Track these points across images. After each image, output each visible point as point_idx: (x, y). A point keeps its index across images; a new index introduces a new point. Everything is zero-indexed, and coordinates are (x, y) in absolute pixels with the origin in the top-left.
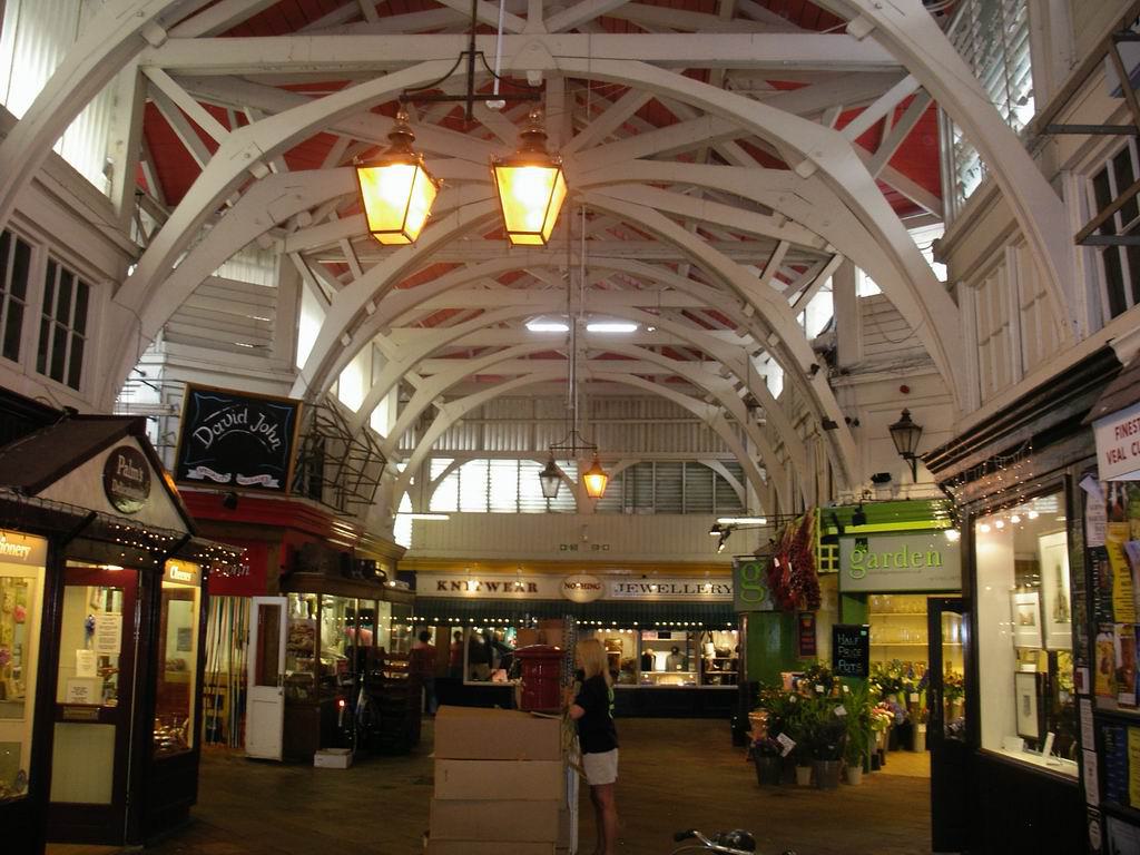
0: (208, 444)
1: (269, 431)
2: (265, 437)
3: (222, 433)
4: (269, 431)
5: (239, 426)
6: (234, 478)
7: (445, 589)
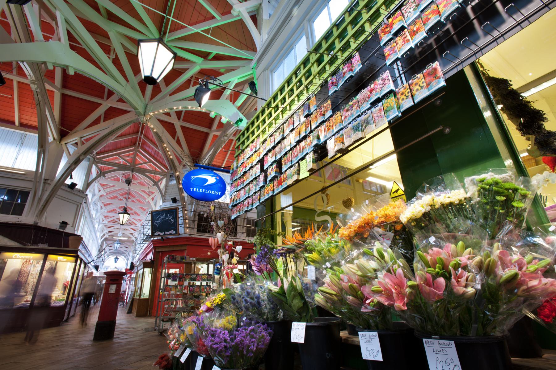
0: (158, 225)
1: (171, 218)
2: (170, 220)
4: (171, 218)
5: (164, 219)
6: (165, 233)
7: (196, 77)
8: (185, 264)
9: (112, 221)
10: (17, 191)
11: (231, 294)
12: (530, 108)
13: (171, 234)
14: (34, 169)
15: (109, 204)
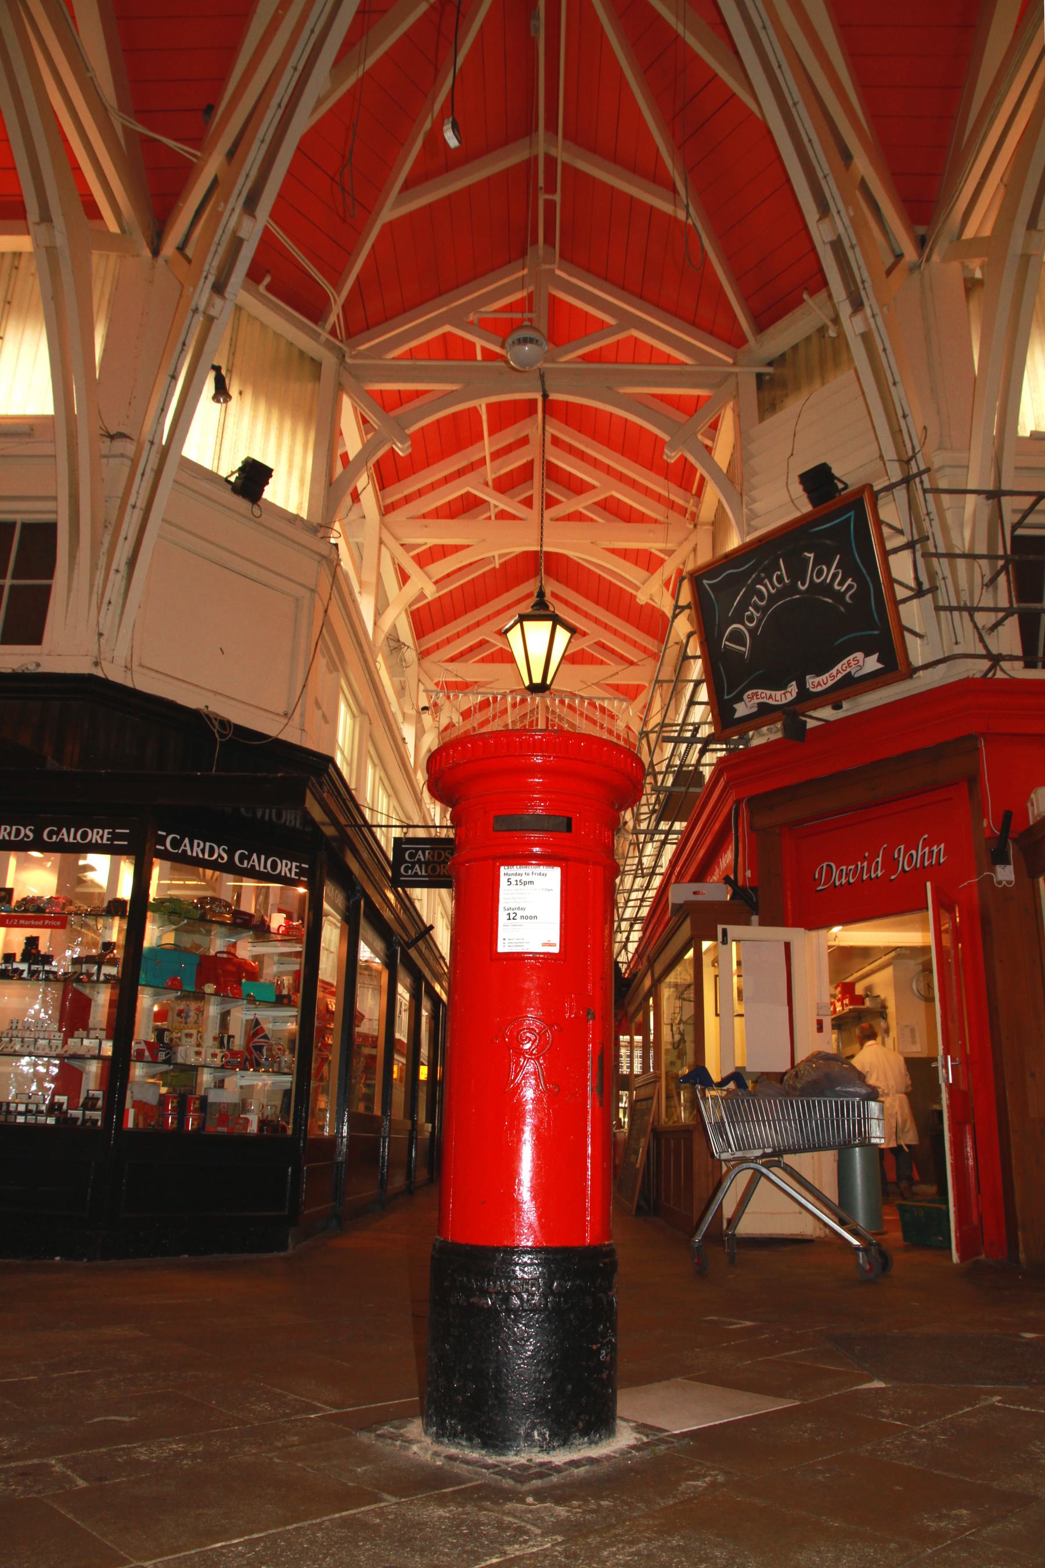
0: (745, 650)
1: (830, 573)
2: (826, 589)
3: (760, 621)
4: (830, 573)
5: (780, 594)
6: (802, 685)
9: (471, 649)
10: (12, 525)
13: (850, 685)
15: (514, 517)
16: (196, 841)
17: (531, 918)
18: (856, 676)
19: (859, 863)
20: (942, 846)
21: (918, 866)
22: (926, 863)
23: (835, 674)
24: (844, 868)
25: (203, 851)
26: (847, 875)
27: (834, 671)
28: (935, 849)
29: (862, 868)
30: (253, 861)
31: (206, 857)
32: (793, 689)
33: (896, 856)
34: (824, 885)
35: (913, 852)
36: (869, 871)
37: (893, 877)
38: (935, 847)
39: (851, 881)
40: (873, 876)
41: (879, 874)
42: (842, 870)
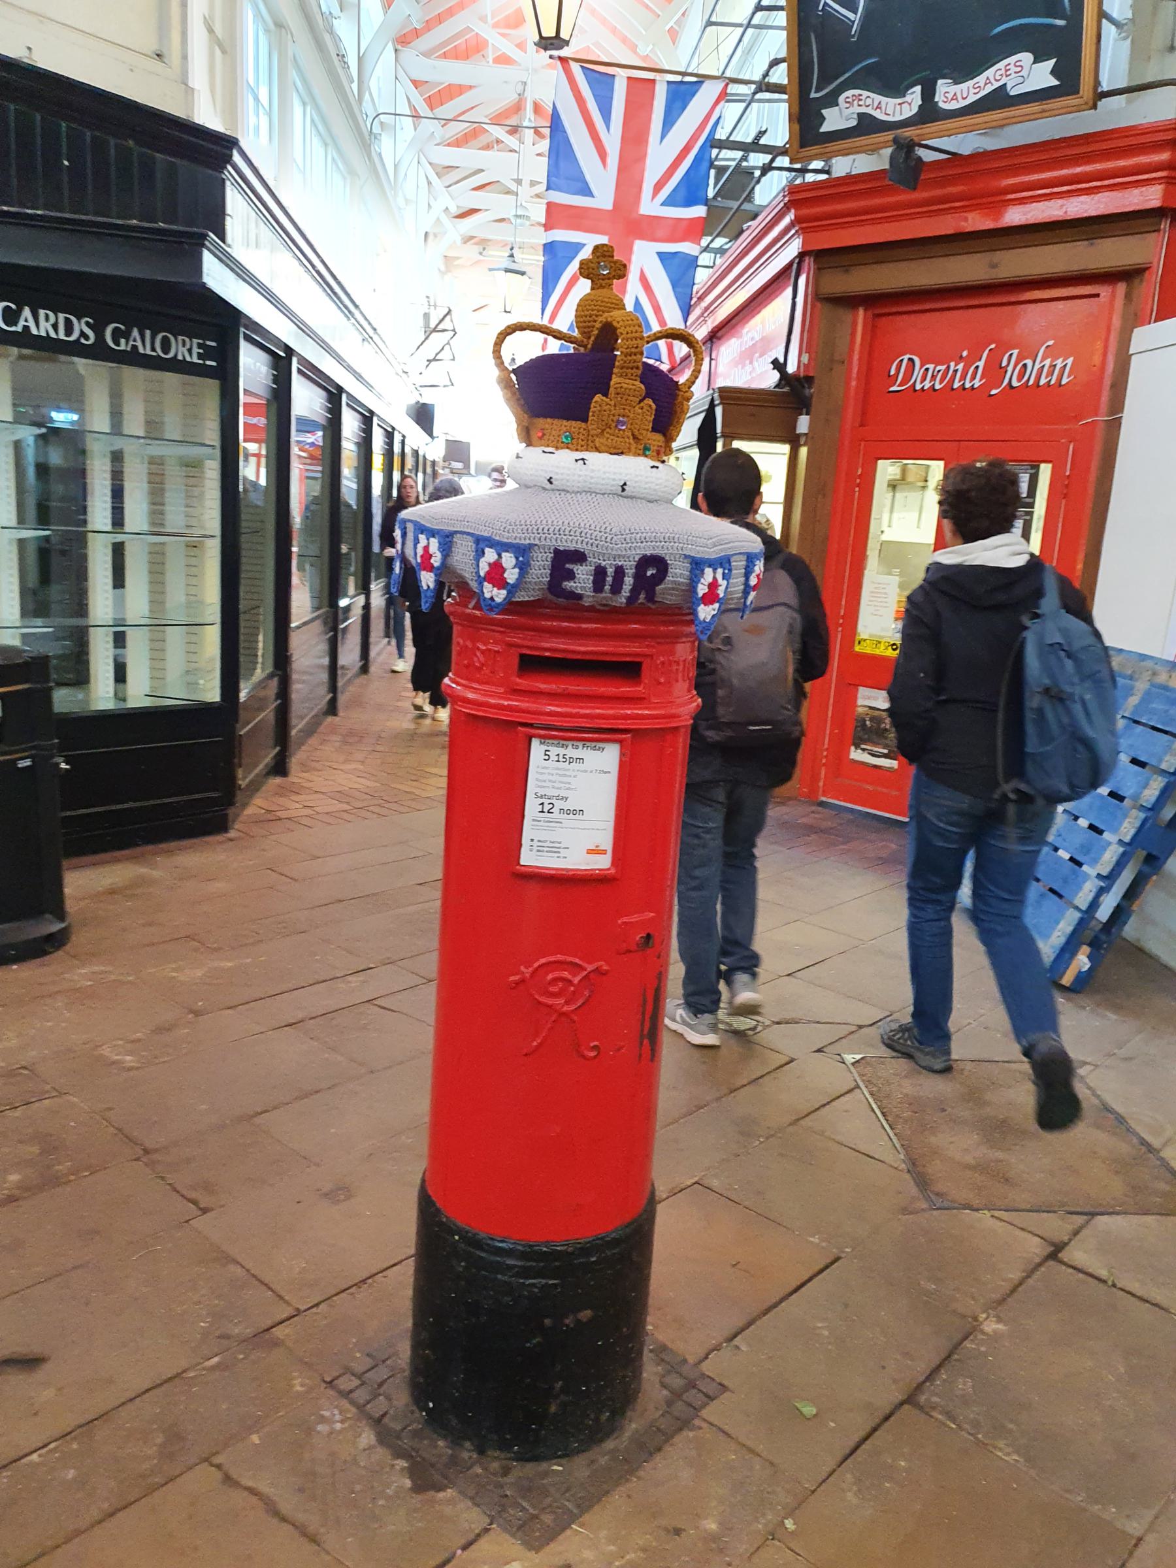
6: (928, 95)
8: (861, 312)
11: (81, 589)
12: (754, 498)
14: (522, 863)
16: (42, 312)
17: (575, 812)
18: (1012, 93)
19: (952, 364)
20: (1070, 361)
21: (1031, 383)
22: (1043, 381)
23: (982, 84)
24: (931, 366)
25: (55, 327)
26: (933, 377)
27: (981, 79)
28: (1059, 363)
29: (956, 371)
30: (135, 340)
31: (62, 336)
32: (915, 96)
33: (1004, 363)
34: (899, 386)
35: (1029, 362)
36: (963, 378)
37: (994, 392)
38: (1061, 360)
39: (938, 387)
40: (968, 385)
41: (977, 383)
42: (927, 369)
